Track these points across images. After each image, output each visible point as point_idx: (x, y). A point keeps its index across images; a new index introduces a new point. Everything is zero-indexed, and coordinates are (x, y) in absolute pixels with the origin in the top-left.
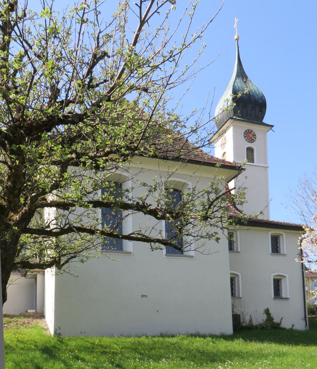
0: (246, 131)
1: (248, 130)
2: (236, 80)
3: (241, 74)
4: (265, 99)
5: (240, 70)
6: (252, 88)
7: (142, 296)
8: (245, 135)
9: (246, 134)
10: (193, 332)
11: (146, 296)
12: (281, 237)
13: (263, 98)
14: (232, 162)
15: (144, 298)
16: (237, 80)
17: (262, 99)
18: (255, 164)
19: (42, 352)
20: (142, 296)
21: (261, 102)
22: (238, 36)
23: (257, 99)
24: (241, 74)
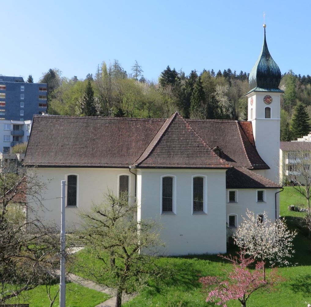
0: (265, 97)
1: (267, 96)
2: (261, 59)
3: (266, 54)
4: (280, 72)
5: (266, 50)
6: (271, 65)
7: (181, 235)
8: (268, 96)
9: (265, 99)
10: (171, 255)
11: (182, 235)
12: (264, 192)
13: (279, 72)
14: (282, 74)
15: (181, 236)
16: (262, 60)
17: (278, 72)
18: (271, 118)
19: (97, 74)
20: (181, 235)
21: (277, 75)
22: (265, 25)
23: (274, 73)
24: (266, 54)
